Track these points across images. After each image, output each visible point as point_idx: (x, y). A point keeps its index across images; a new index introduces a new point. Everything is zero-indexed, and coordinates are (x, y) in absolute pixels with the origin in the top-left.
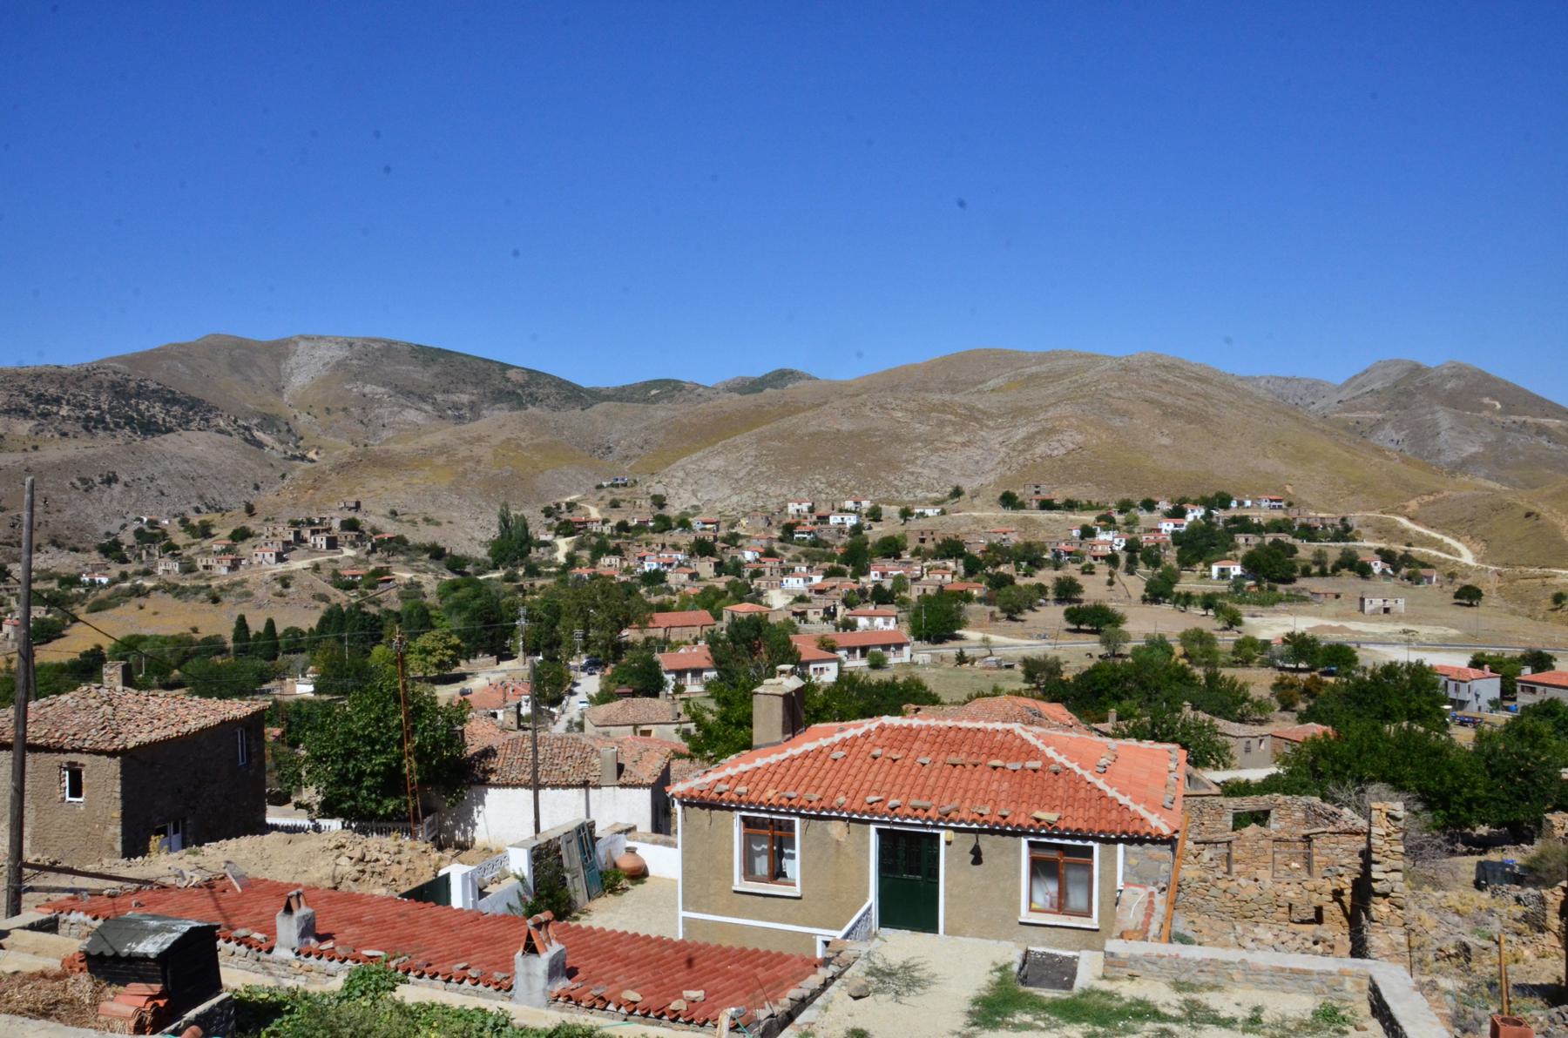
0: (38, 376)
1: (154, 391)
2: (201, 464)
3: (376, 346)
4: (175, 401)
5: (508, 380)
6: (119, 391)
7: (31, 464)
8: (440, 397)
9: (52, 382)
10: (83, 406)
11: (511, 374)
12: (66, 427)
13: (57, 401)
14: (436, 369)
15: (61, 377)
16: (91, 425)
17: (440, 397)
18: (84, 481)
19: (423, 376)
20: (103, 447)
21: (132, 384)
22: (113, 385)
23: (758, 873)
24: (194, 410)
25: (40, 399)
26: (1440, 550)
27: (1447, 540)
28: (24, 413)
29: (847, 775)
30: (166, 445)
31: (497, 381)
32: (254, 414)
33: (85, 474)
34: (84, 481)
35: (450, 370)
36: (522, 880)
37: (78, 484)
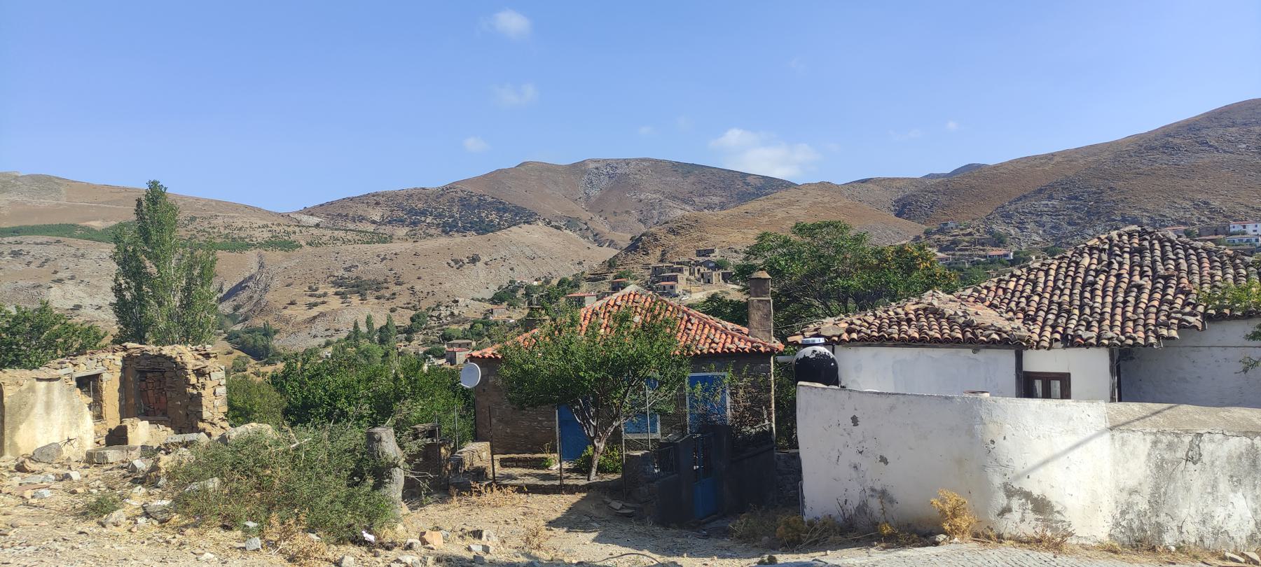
0: (410, 196)
1: (490, 203)
2: (539, 248)
3: (646, 164)
4: (505, 210)
5: (748, 184)
6: (465, 203)
7: (419, 250)
8: (697, 200)
9: (419, 199)
10: (440, 216)
11: (749, 179)
12: (432, 231)
13: (424, 213)
14: (692, 179)
15: (423, 194)
16: (448, 229)
17: (697, 200)
18: (456, 262)
19: (686, 185)
20: (463, 243)
21: (475, 199)
22: (461, 199)
23: (1058, 383)
24: (523, 216)
25: (412, 212)
28: (401, 222)
29: (1125, 302)
30: (512, 234)
31: (739, 185)
32: (561, 218)
33: (455, 257)
34: (456, 262)
35: (703, 179)
37: (452, 264)
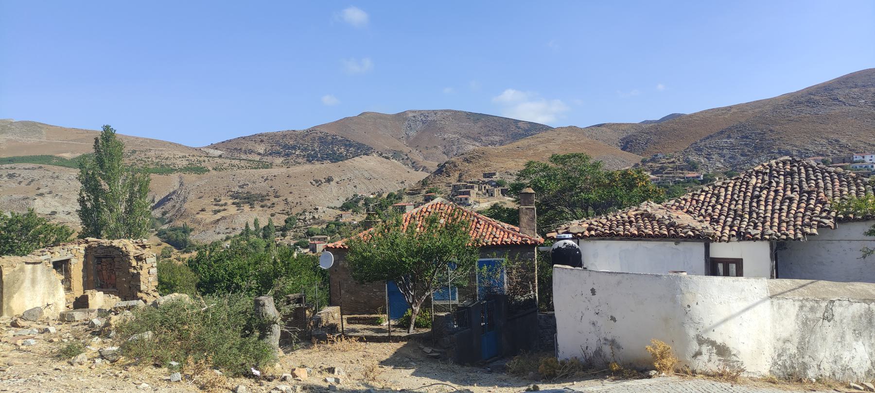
0: (285, 136)
1: (340, 141)
2: (374, 172)
3: (448, 114)
4: (351, 146)
5: (519, 128)
6: (323, 141)
7: (290, 173)
8: (483, 138)
9: (291, 138)
10: (305, 149)
11: (520, 124)
12: (300, 160)
13: (294, 148)
14: (480, 124)
15: (293, 134)
16: (311, 159)
17: (483, 138)
18: (317, 181)
19: (476, 128)
20: (321, 168)
21: (329, 138)
22: (320, 138)
24: (363, 150)
25: (286, 147)
26: (360, 319)
27: (457, 294)
28: (278, 154)
30: (355, 162)
31: (513, 128)
32: (389, 151)
33: (316, 178)
34: (317, 181)
35: (488, 124)
36: (706, 331)
37: (314, 183)
